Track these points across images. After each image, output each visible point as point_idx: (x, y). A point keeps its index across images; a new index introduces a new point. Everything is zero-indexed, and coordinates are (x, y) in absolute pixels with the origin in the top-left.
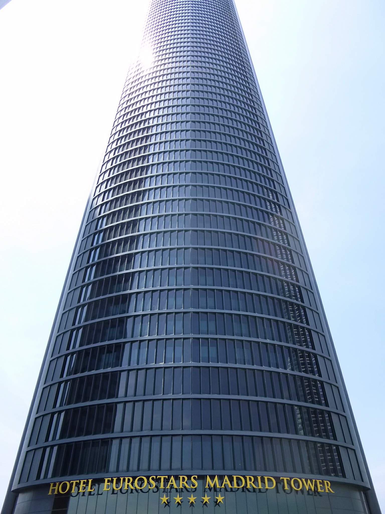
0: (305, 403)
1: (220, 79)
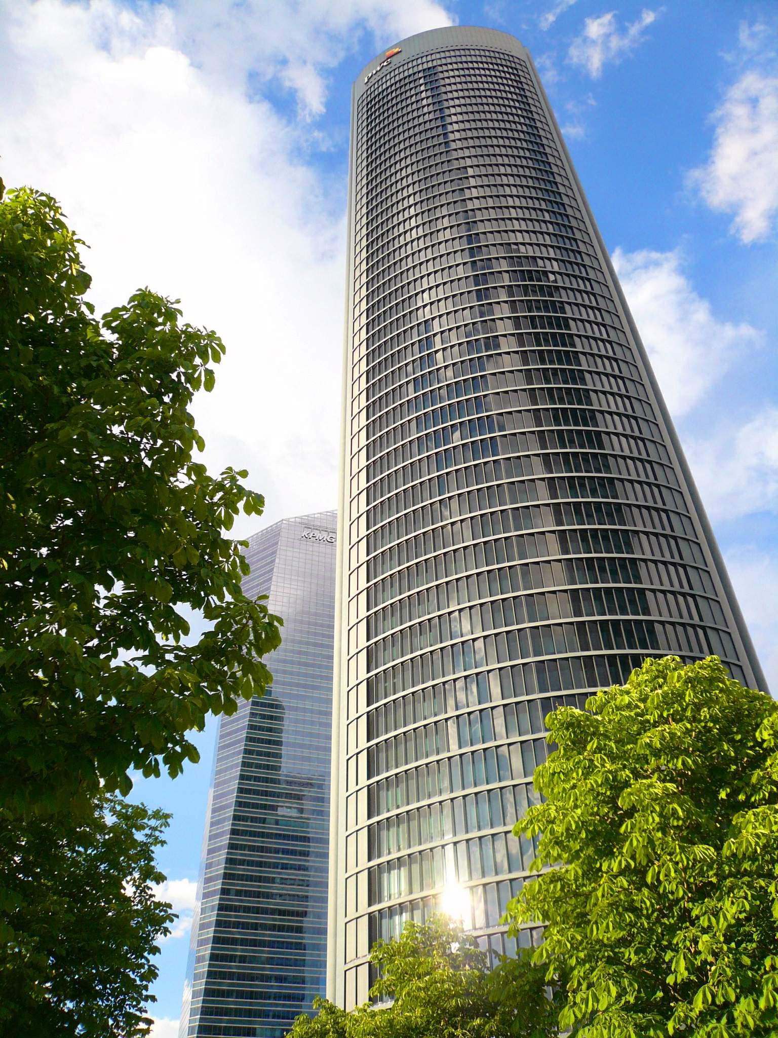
0: (187, 954)
1: (497, 87)
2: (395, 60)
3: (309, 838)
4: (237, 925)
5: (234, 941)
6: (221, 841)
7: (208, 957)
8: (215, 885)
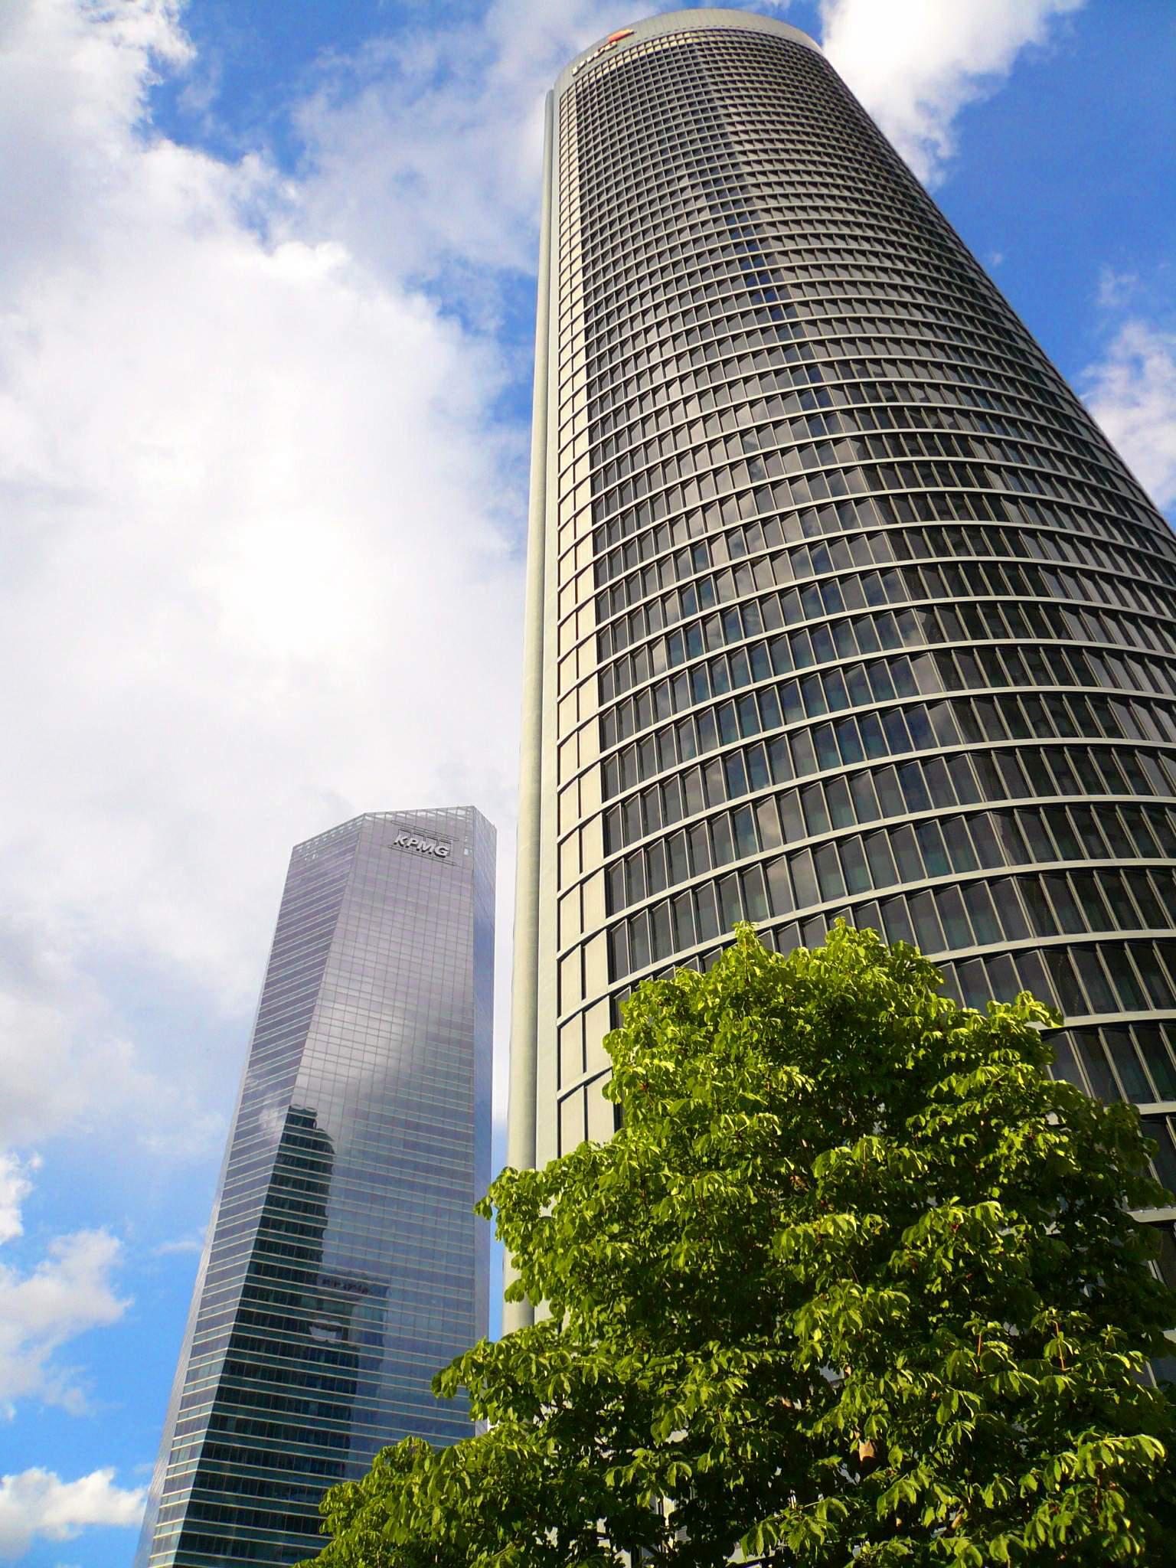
2: (624, 44)
3: (348, 1438)
4: (233, 1485)
5: (226, 1515)
6: (224, 1307)
7: (175, 1541)
8: (200, 1410)
